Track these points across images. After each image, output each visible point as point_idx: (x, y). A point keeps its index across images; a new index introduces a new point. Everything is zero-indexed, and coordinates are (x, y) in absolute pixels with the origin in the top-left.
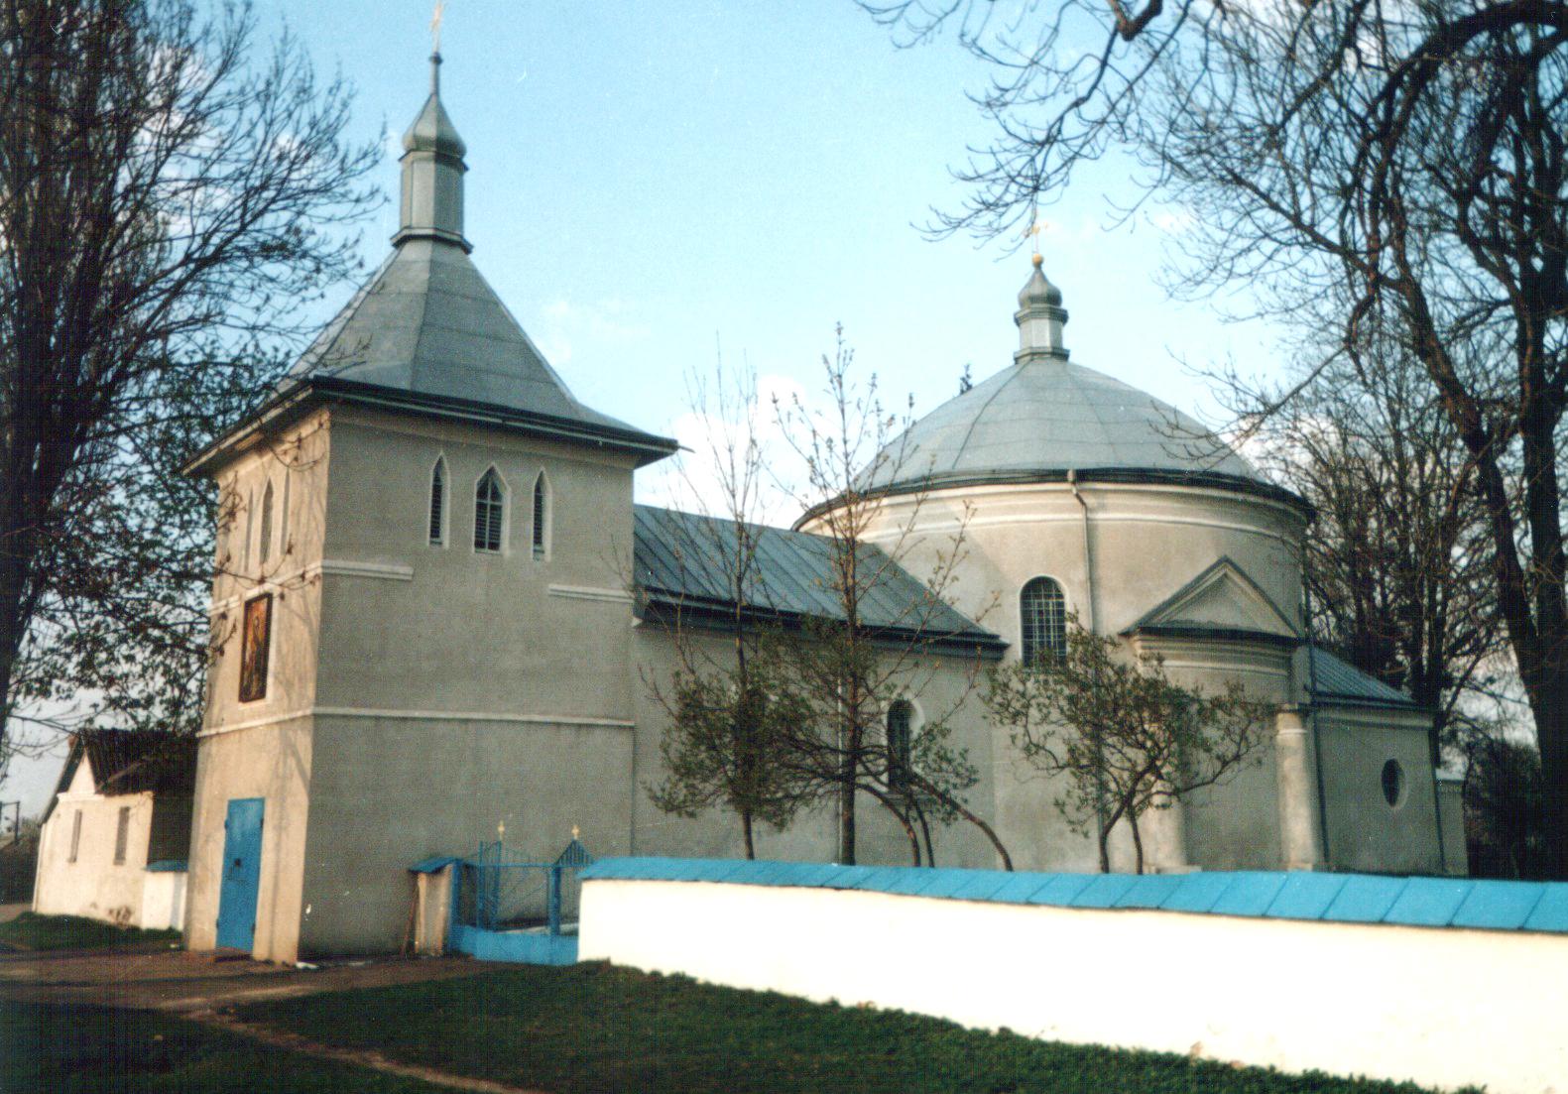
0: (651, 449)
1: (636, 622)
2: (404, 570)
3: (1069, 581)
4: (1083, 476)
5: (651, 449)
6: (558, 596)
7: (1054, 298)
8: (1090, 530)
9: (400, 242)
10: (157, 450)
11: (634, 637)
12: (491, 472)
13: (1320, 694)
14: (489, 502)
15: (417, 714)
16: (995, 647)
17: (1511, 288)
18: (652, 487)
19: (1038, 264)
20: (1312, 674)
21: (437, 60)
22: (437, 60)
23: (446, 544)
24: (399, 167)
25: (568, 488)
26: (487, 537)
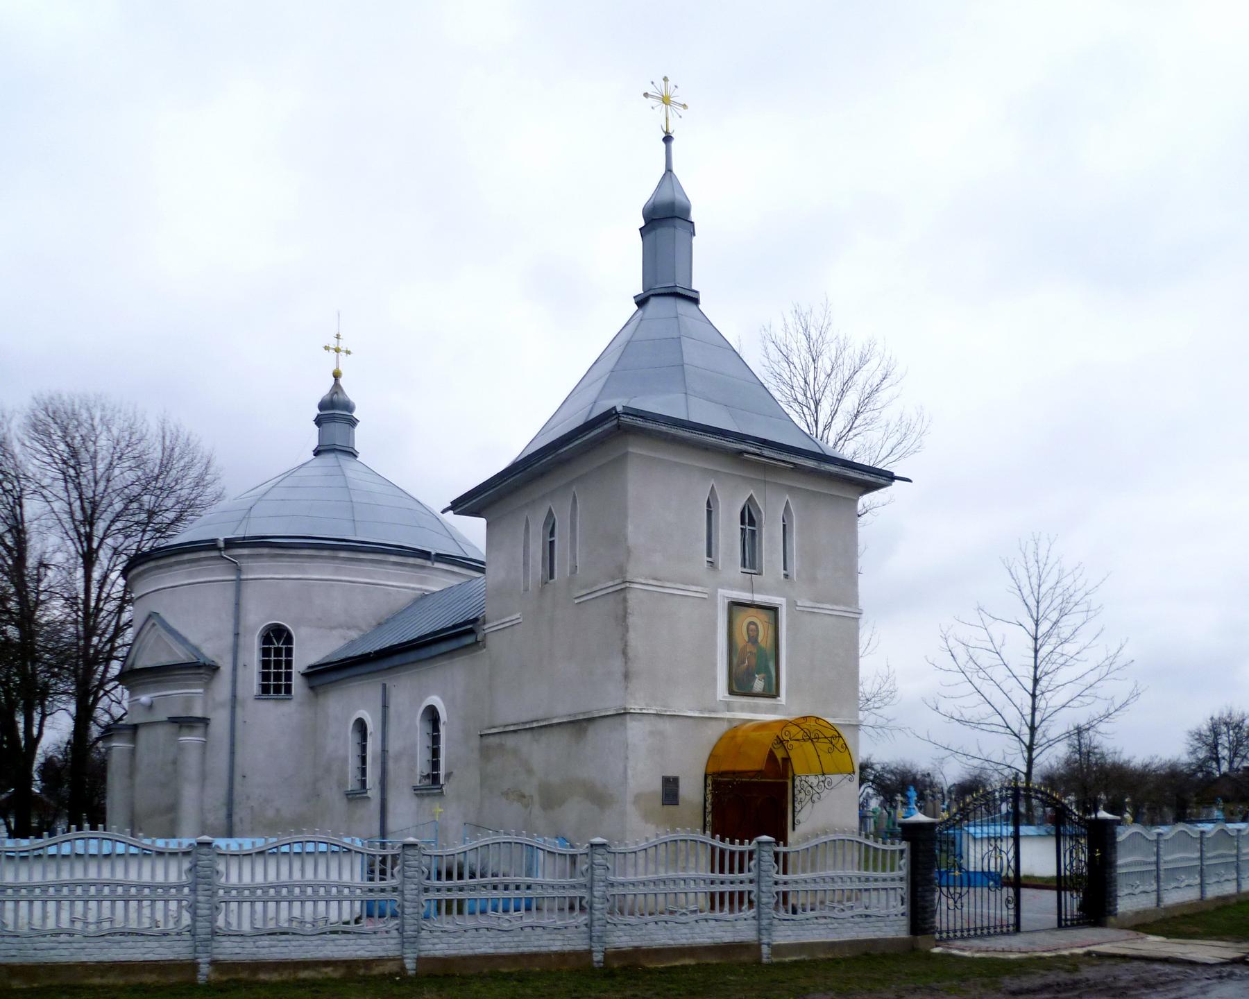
9: (641, 302)
12: (751, 499)
19: (337, 376)
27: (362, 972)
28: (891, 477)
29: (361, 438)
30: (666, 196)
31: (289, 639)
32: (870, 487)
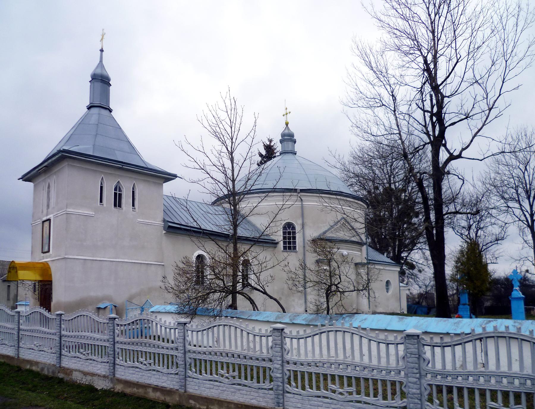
0: (168, 177)
1: (164, 232)
2: (91, 213)
3: (297, 224)
4: (302, 191)
5: (168, 177)
6: (140, 223)
7: (291, 135)
8: (302, 207)
9: (89, 108)
10: (415, 220)
11: (164, 238)
12: (118, 182)
13: (370, 260)
14: (118, 192)
15: (70, 257)
16: (274, 244)
17: (430, 138)
18: (168, 188)
19: (287, 124)
20: (367, 254)
21: (102, 51)
22: (102, 51)
23: (105, 205)
24: (89, 84)
25: (143, 189)
26: (118, 202)
27: (28, 367)
28: (175, 176)
29: (297, 147)
30: (99, 71)
31: (294, 228)
32: (167, 180)
